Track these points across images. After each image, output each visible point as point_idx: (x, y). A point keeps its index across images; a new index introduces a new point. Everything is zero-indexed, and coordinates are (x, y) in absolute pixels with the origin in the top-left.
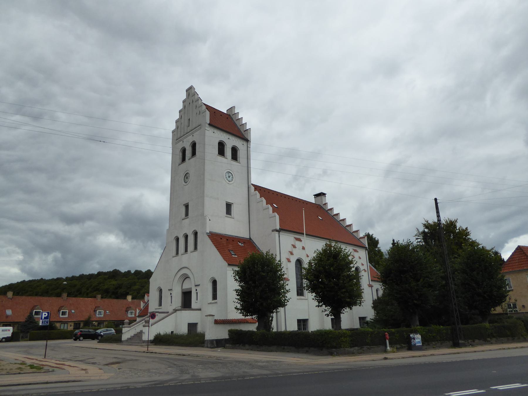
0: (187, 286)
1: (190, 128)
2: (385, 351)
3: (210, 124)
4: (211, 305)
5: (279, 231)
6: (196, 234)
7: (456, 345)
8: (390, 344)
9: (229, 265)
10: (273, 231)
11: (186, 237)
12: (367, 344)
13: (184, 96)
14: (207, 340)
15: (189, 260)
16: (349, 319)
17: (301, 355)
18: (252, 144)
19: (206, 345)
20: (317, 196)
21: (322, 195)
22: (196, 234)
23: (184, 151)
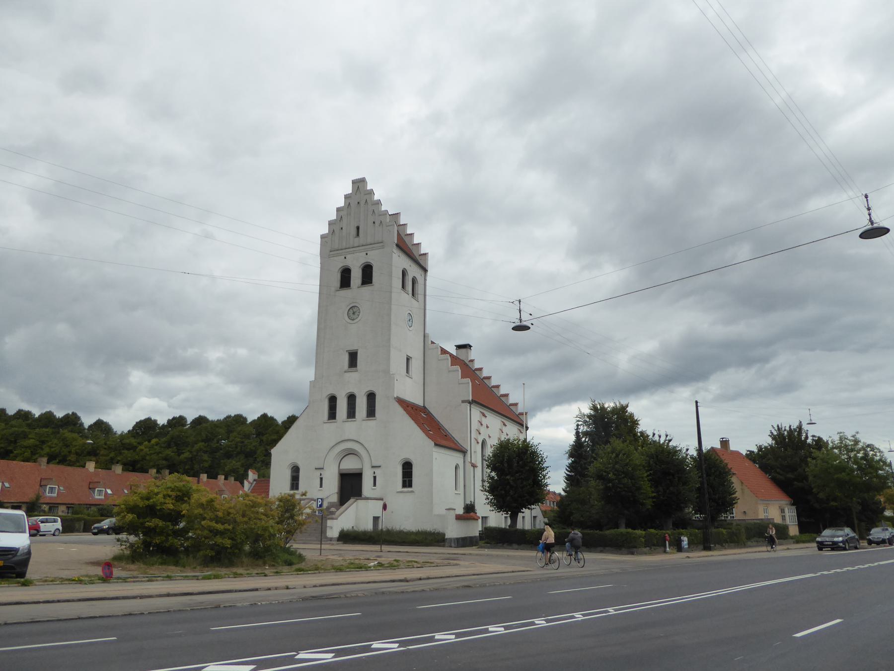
0: (350, 465)
1: (357, 241)
2: (665, 552)
3: (397, 245)
4: (402, 495)
5: (470, 403)
6: (371, 397)
7: (707, 548)
8: (670, 545)
9: (436, 445)
10: (463, 402)
11: (352, 398)
12: (654, 545)
13: (349, 190)
14: (450, 539)
15: (360, 429)
16: (528, 518)
17: (622, 554)
18: (429, 273)
19: (447, 544)
20: (459, 347)
21: (467, 347)
22: (371, 397)
23: (346, 274)
